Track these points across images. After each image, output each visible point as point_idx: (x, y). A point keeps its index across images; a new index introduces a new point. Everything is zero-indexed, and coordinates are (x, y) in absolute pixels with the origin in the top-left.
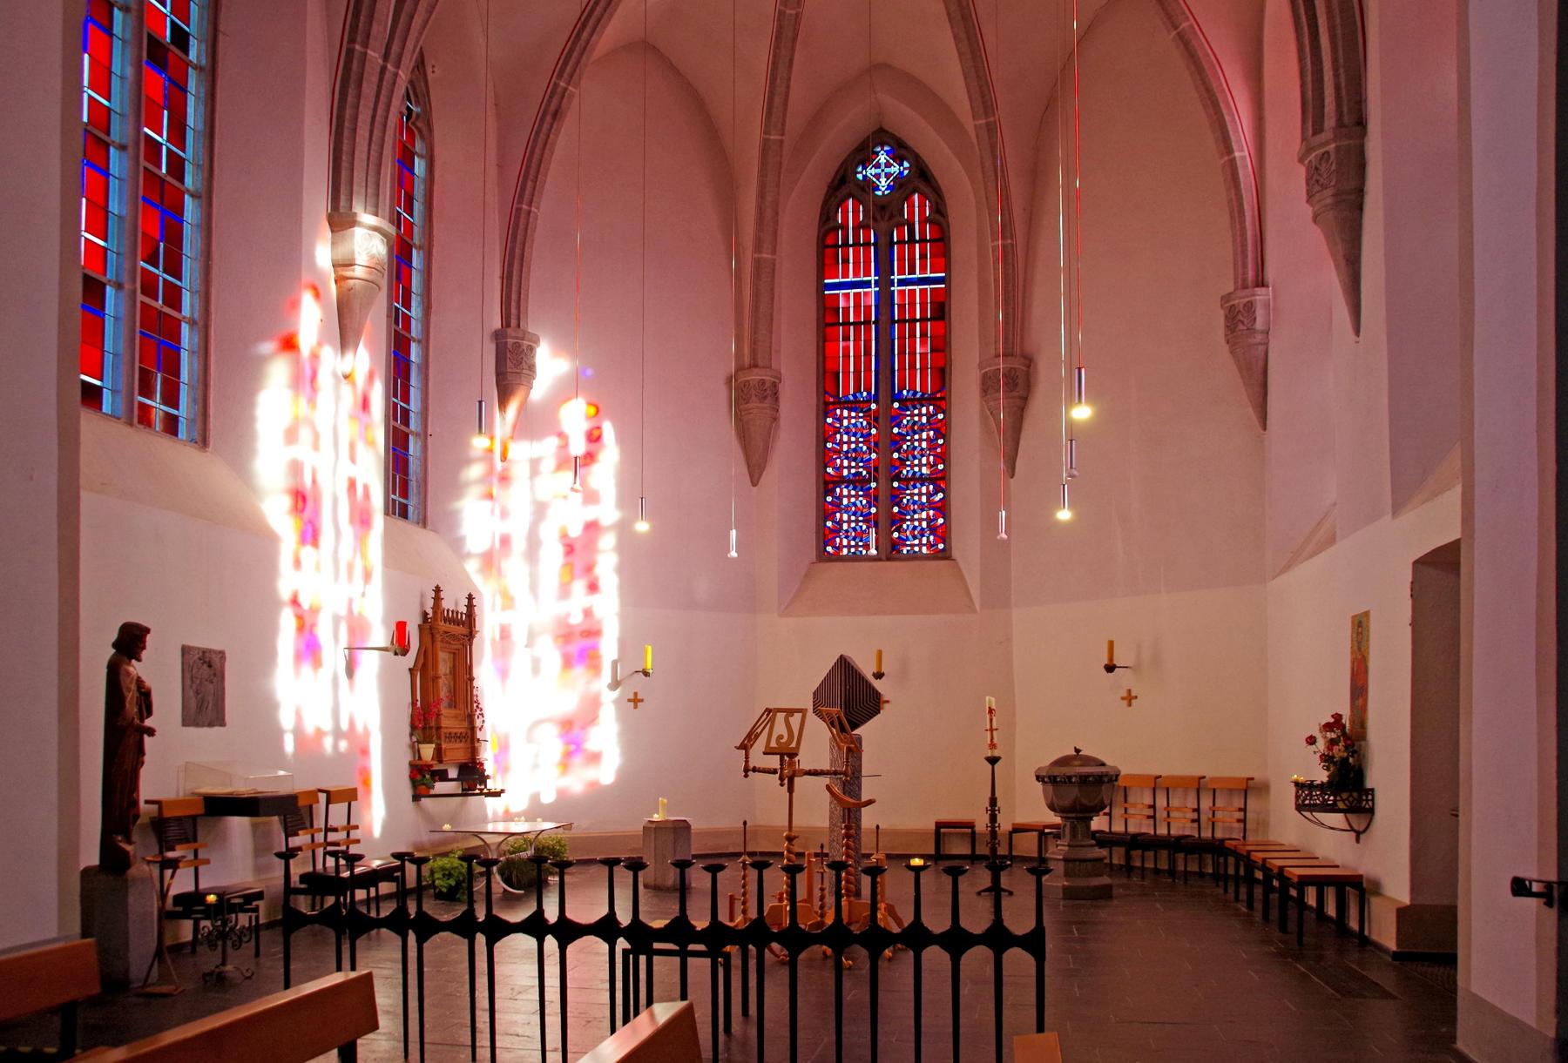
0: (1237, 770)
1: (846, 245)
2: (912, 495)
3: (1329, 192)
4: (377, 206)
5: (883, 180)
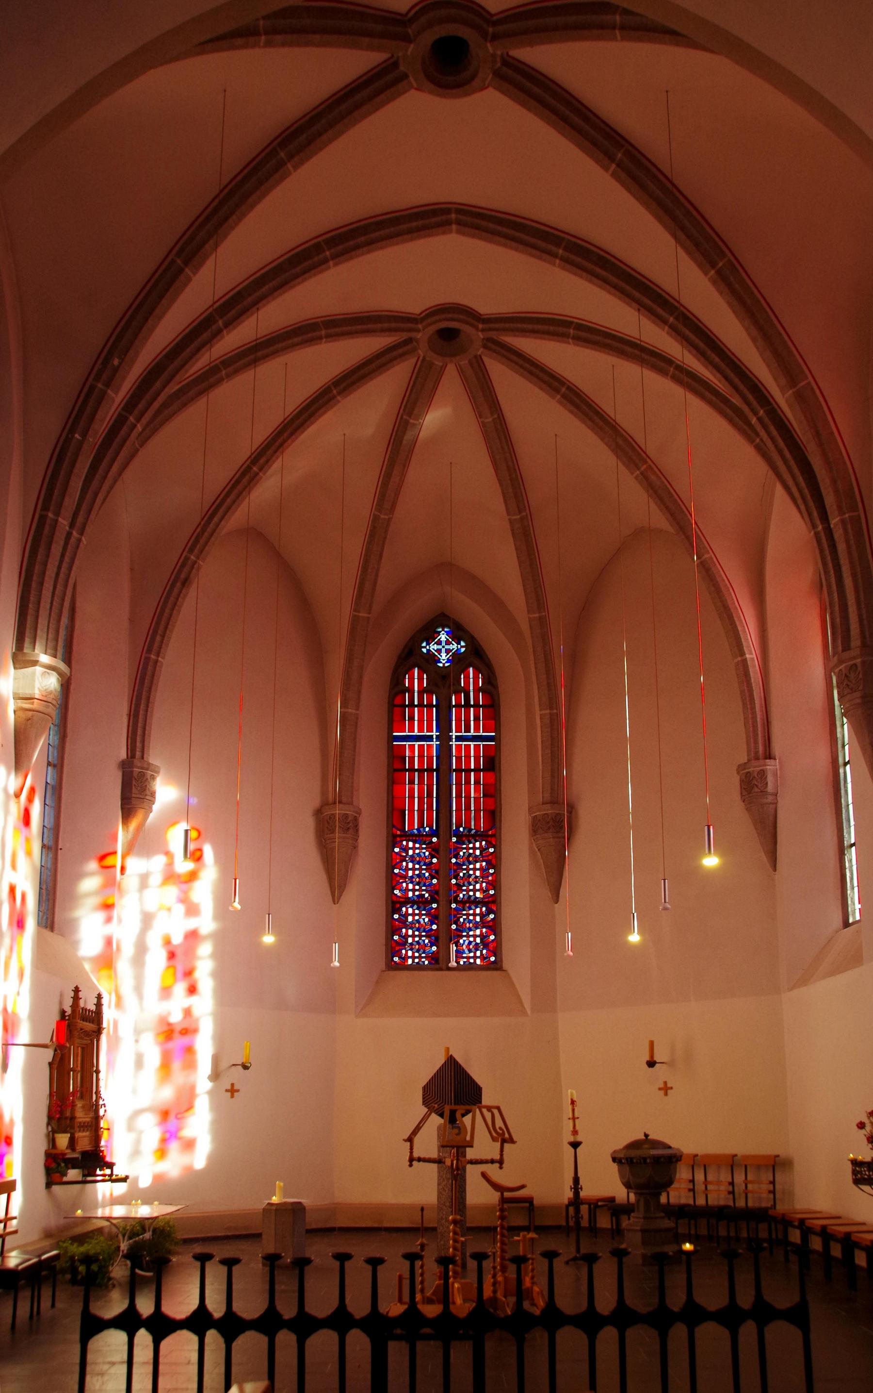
0: (766, 1149)
1: (412, 705)
2: (468, 915)
3: (858, 694)
4: (56, 649)
5: (444, 654)
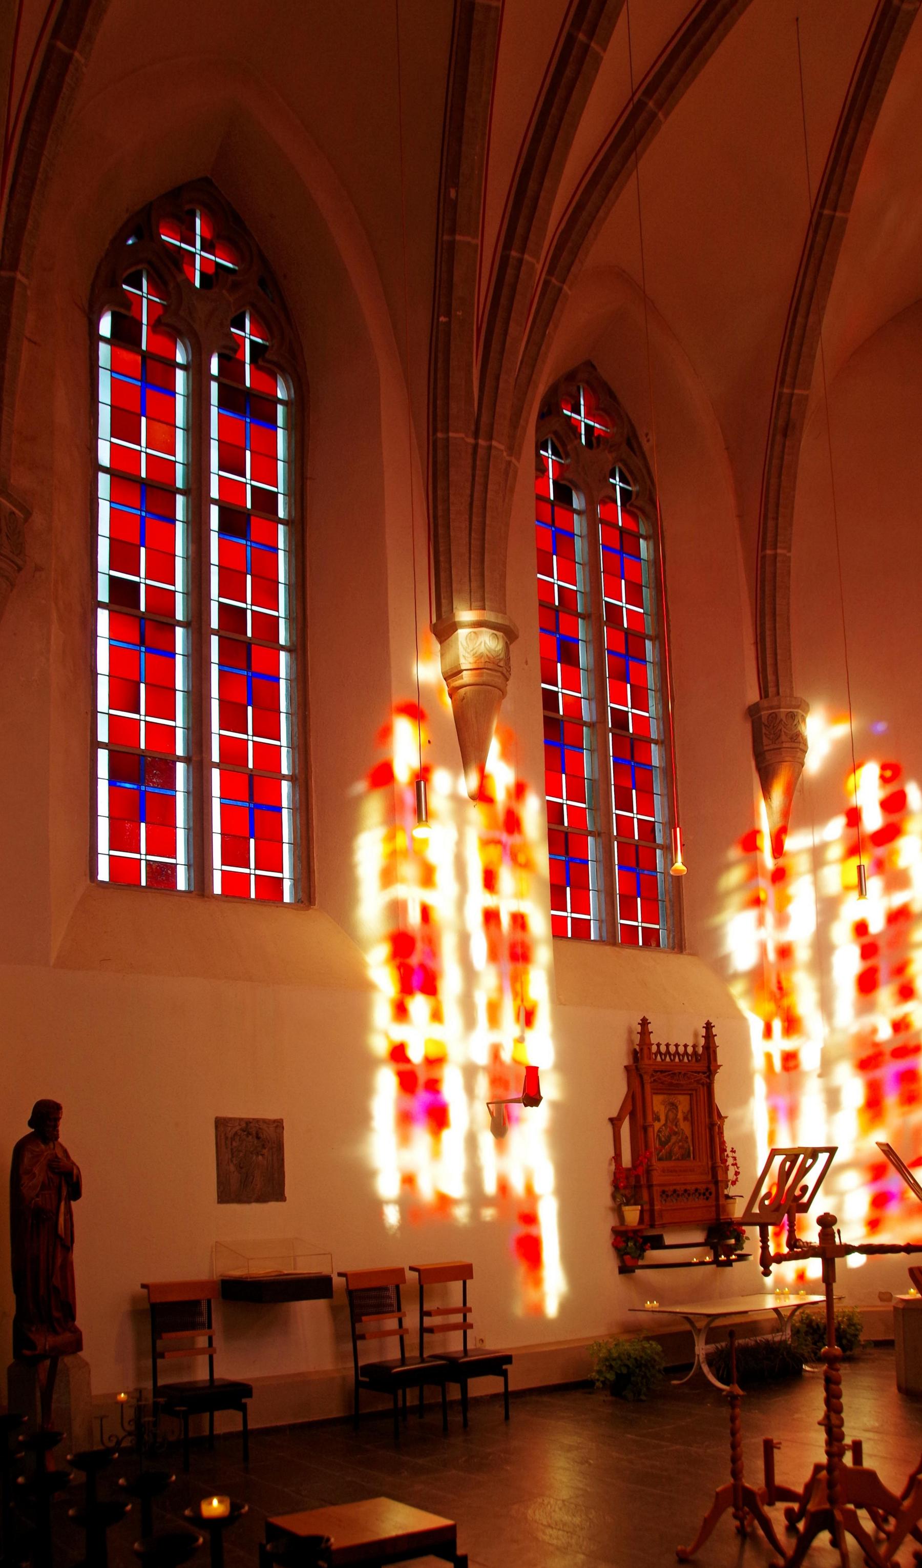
4: (483, 599)
